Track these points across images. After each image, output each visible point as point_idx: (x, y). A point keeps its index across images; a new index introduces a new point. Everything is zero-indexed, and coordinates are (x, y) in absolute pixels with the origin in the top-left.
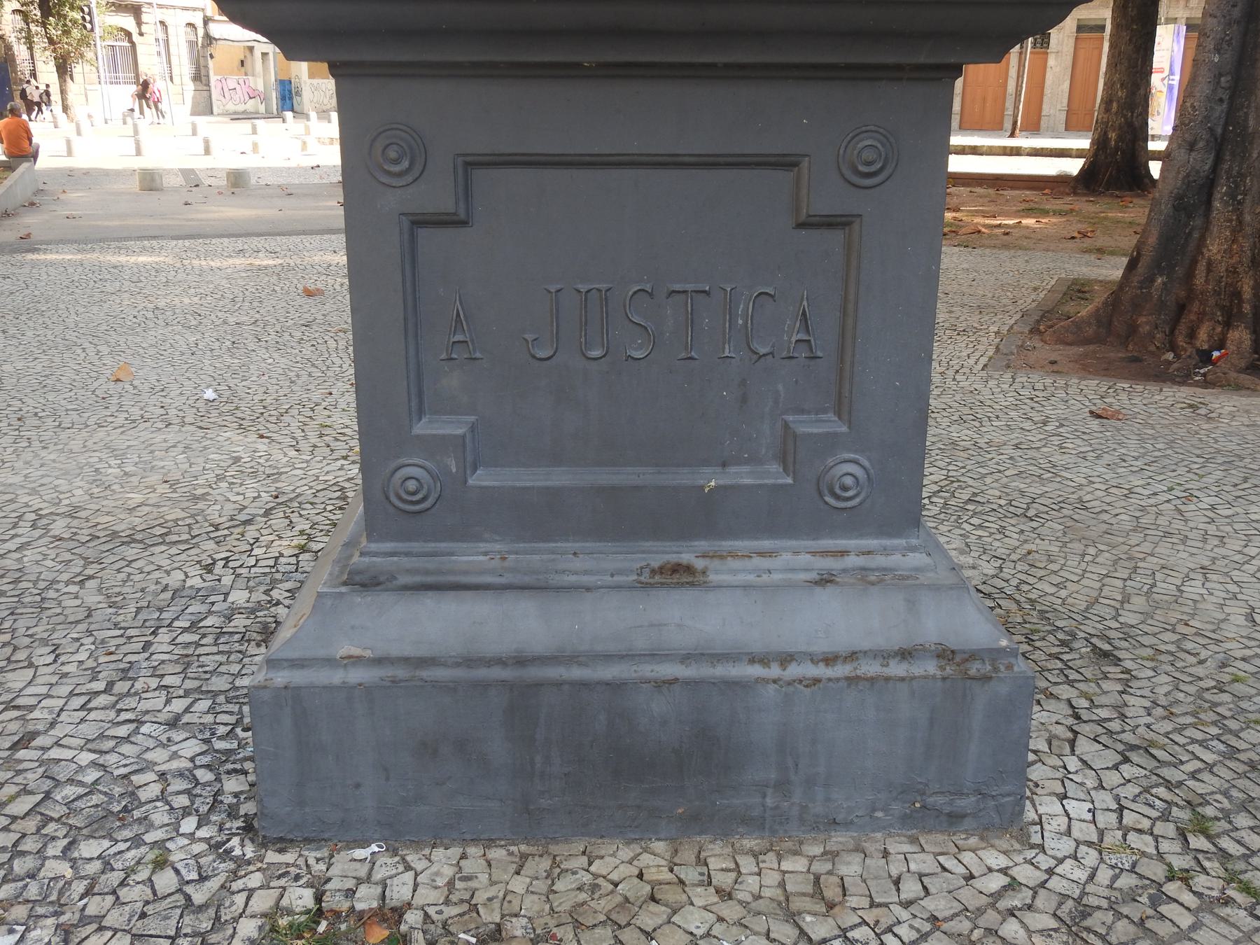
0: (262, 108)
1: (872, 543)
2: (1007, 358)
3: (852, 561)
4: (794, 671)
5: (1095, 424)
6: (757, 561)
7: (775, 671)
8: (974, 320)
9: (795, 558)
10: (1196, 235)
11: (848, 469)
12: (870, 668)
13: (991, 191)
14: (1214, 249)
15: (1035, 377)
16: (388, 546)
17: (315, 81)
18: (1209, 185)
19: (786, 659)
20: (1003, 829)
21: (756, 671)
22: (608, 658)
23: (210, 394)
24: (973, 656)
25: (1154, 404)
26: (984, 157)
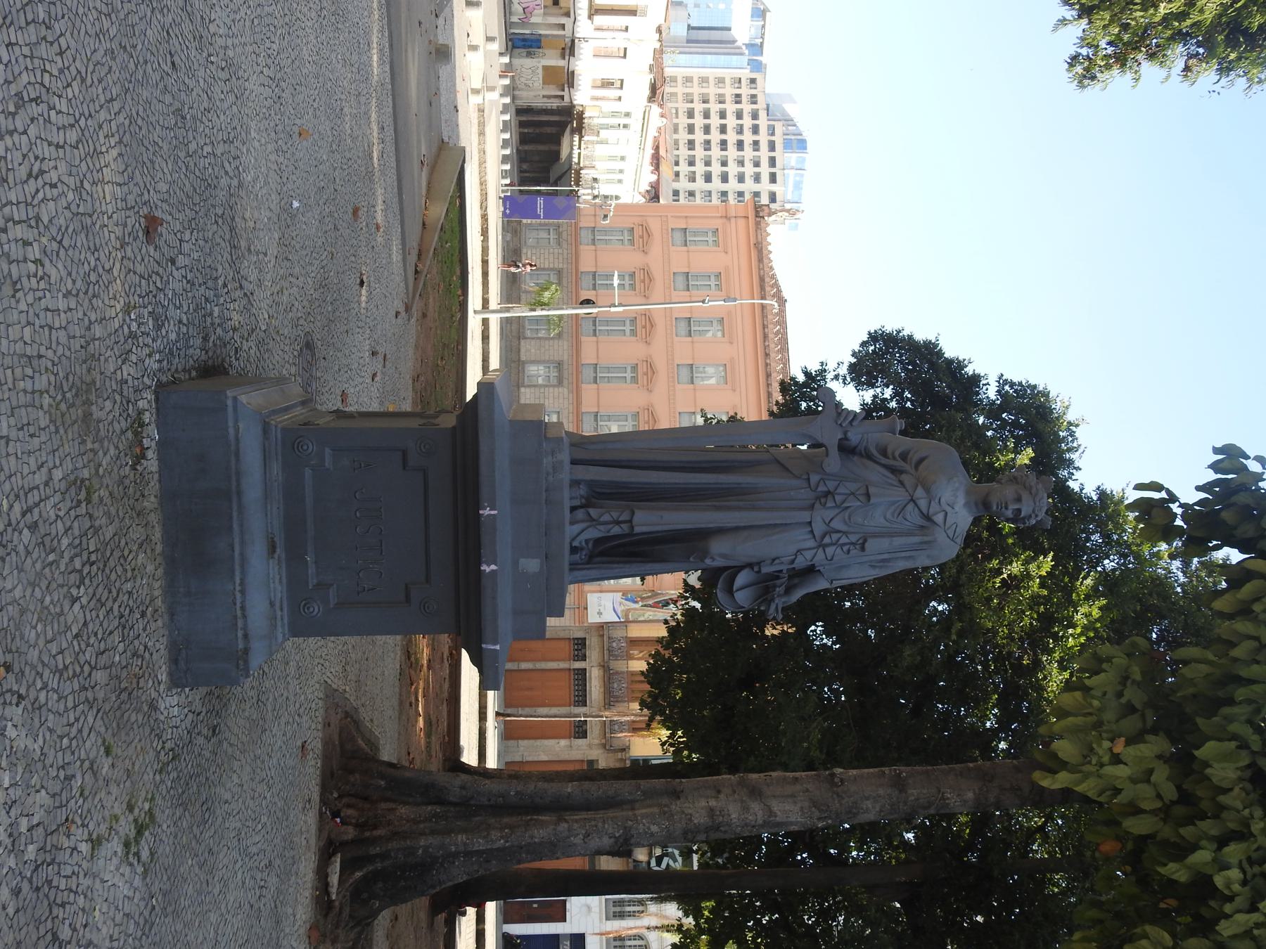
0: (515, 19)
1: (286, 621)
2: (332, 697)
3: (279, 613)
4: (238, 595)
5: (299, 743)
6: (278, 577)
7: (238, 588)
8: (352, 677)
9: (279, 590)
10: (411, 800)
11: (316, 609)
12: (240, 623)
13: (446, 695)
14: (403, 811)
15: (322, 711)
16: (279, 436)
17: (540, 71)
18: (440, 802)
19: (243, 592)
20: (171, 680)
21: (238, 581)
22: (241, 525)
23: (296, 204)
24: (246, 662)
25: (312, 770)
26: (477, 690)
